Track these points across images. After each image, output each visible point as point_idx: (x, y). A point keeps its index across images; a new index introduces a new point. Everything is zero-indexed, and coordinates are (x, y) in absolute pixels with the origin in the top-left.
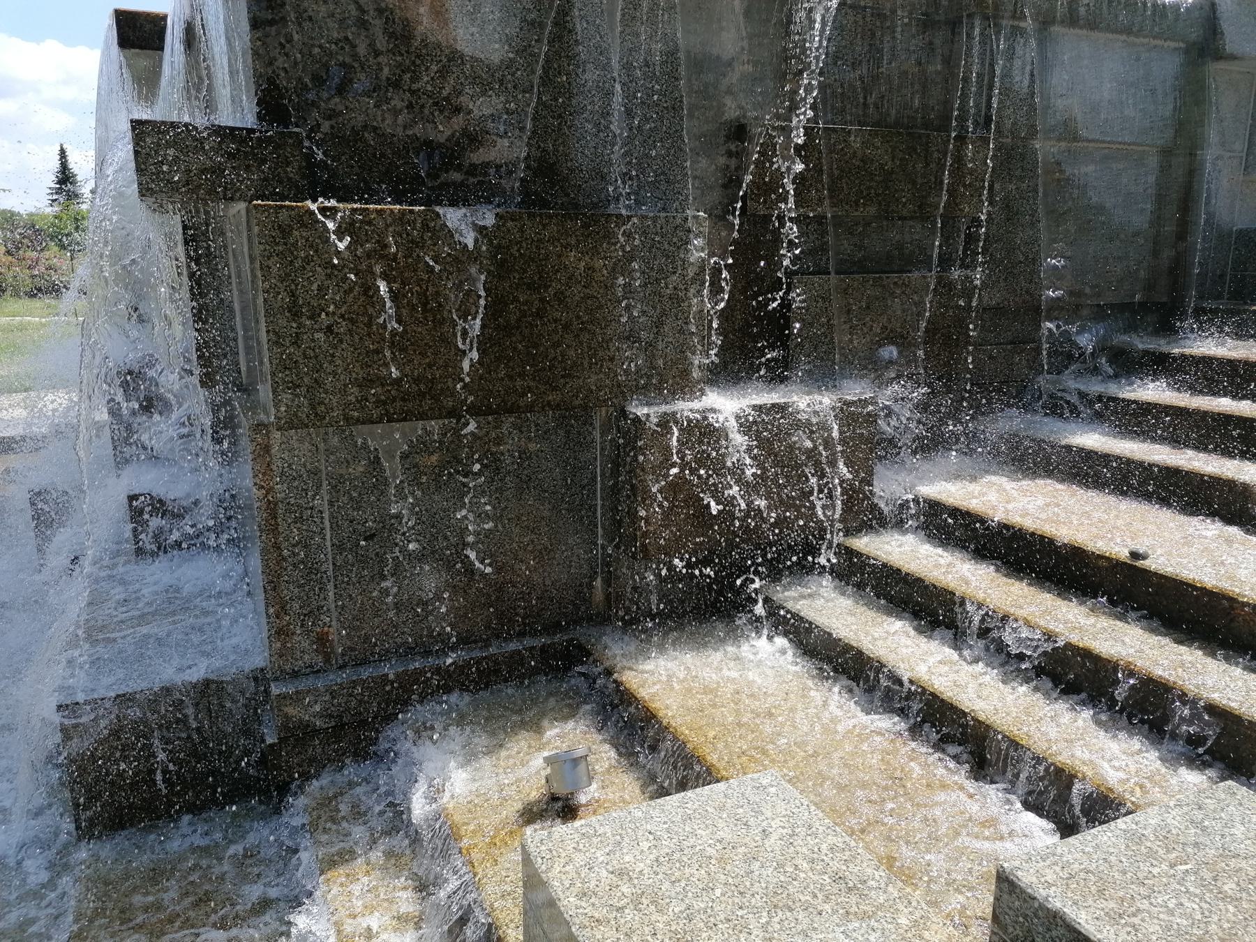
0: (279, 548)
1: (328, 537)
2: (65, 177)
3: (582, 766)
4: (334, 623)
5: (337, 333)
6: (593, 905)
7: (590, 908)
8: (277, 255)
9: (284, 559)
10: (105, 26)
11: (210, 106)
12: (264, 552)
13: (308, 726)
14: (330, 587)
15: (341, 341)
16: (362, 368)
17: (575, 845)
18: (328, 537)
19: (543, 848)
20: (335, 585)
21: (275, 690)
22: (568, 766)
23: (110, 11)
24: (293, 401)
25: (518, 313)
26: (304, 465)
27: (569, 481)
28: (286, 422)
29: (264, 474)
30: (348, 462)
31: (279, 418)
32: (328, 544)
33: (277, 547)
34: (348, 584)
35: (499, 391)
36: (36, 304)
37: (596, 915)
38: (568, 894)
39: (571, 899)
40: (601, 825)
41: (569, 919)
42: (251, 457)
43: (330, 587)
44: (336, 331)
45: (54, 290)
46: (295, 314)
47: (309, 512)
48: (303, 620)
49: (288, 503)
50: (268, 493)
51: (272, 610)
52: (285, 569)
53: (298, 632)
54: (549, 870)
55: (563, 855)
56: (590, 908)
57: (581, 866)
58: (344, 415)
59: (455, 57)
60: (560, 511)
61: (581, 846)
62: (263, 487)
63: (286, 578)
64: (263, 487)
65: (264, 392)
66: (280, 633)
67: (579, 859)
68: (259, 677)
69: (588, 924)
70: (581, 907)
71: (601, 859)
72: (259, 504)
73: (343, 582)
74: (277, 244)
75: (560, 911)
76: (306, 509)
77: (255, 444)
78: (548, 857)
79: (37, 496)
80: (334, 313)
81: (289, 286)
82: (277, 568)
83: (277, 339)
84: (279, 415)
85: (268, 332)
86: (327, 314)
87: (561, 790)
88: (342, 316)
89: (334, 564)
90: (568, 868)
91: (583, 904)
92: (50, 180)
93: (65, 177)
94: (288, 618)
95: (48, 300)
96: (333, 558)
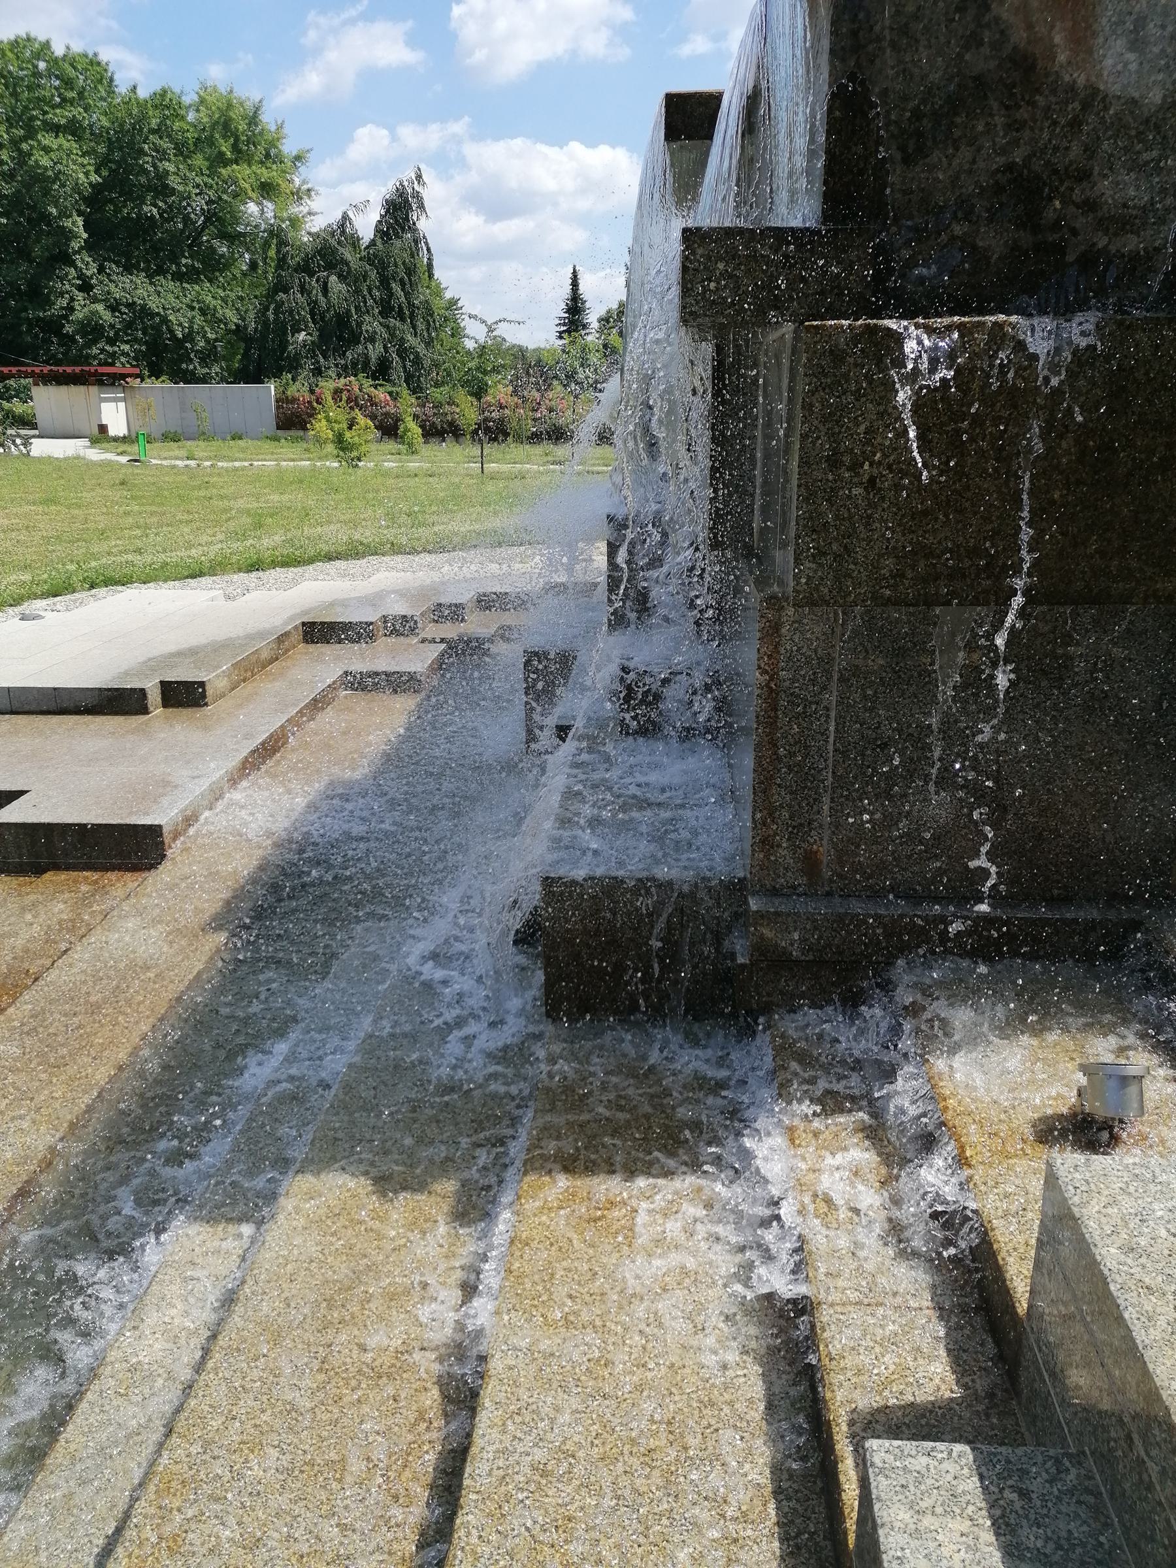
0: (775, 745)
1: (831, 739)
2: (575, 308)
3: (1133, 1089)
4: (825, 842)
5: (880, 489)
6: (1144, 1267)
7: (1139, 1269)
8: (824, 389)
9: (779, 759)
10: (653, 114)
11: (768, 203)
12: (758, 747)
13: (784, 953)
14: (826, 799)
15: (883, 499)
16: (904, 535)
17: (1123, 1186)
18: (831, 739)
19: (1077, 1175)
20: (832, 799)
21: (754, 904)
22: (1113, 1083)
23: (662, 96)
24: (815, 571)
25: (1130, 463)
26: (816, 651)
27: (1165, 705)
28: (804, 597)
29: (770, 657)
30: (867, 651)
31: (798, 592)
32: (831, 748)
33: (774, 744)
34: (847, 799)
35: (1084, 573)
36: (537, 450)
37: (1147, 1280)
38: (1109, 1242)
39: (1113, 1251)
40: (1164, 1171)
41: (1106, 1272)
42: (758, 635)
43: (826, 799)
44: (878, 485)
45: (558, 435)
46: (834, 462)
47: (814, 707)
48: (791, 832)
49: (792, 694)
50: (772, 679)
51: (758, 815)
52: (779, 771)
53: (784, 845)
54: (1084, 1204)
55: (1106, 1192)
56: (1139, 1269)
57: (1130, 1214)
58: (873, 593)
59: (1093, 98)
60: (1144, 745)
61: (1132, 1189)
62: (766, 672)
63: (778, 781)
64: (766, 672)
65: (783, 558)
66: (765, 843)
67: (1128, 1204)
68: (737, 889)
69: (1133, 1287)
70: (1125, 1264)
71: (1160, 1213)
72: (759, 691)
73: (842, 796)
74: (826, 376)
75: (1095, 1260)
76: (811, 703)
77: (764, 620)
78: (1083, 1188)
79: (533, 657)
80: (880, 463)
81: (832, 429)
82: (771, 768)
83: (809, 494)
84: (798, 588)
85: (799, 486)
86: (871, 465)
87: (1098, 1108)
88: (890, 467)
89: (833, 773)
90: (1109, 1210)
91: (1129, 1261)
92: (558, 309)
93: (575, 308)
94: (775, 827)
95: (547, 446)
96: (834, 766)
